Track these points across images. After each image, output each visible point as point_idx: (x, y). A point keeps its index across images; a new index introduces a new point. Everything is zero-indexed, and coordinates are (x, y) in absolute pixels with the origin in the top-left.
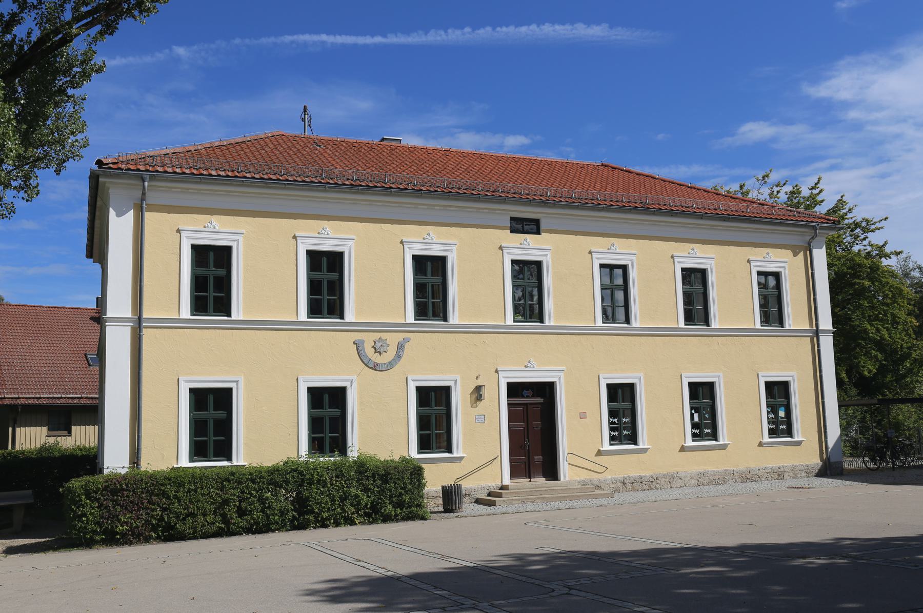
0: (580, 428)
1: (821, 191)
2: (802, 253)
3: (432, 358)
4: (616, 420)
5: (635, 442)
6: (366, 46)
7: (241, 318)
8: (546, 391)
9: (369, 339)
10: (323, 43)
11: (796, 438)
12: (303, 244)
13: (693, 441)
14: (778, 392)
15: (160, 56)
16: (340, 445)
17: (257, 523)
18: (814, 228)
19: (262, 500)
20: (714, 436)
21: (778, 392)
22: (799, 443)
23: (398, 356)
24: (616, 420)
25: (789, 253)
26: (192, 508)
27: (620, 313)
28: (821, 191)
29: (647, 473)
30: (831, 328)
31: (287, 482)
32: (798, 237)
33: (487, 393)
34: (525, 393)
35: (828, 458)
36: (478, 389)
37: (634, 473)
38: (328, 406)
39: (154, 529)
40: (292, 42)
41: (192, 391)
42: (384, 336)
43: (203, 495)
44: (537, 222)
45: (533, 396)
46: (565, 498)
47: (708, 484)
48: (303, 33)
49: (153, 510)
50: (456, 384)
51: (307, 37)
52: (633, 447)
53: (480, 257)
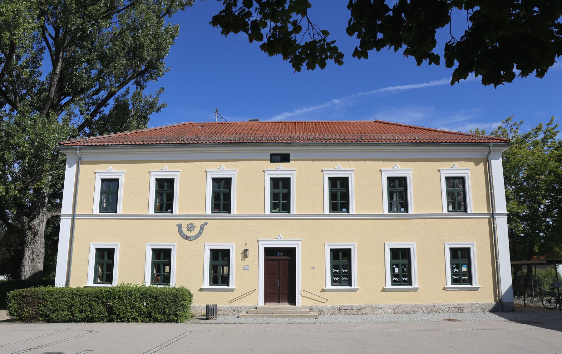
0: (313, 273)
1: (556, 126)
2: (482, 163)
3: (221, 233)
4: (338, 271)
5: (410, 284)
6: (419, 89)
7: (235, 214)
8: (291, 253)
9: (185, 224)
10: (399, 89)
11: (474, 286)
12: (210, 175)
13: (332, 285)
14: (461, 256)
15: (328, 104)
16: (167, 279)
17: (88, 317)
18: (489, 146)
19: (90, 305)
20: (410, 282)
21: (461, 256)
22: (476, 289)
23: (200, 233)
24: (338, 271)
25: (472, 164)
26: (57, 307)
27: (462, 208)
28: (556, 126)
29: (356, 304)
30: (506, 212)
31: (103, 297)
32: (480, 153)
33: (250, 253)
34: (279, 254)
35: (500, 301)
36: (246, 250)
37: (347, 304)
38: (162, 258)
39: (41, 316)
40: (385, 91)
41: (332, 250)
42: (193, 222)
43: (63, 301)
44: (288, 155)
45: (283, 256)
46: (292, 317)
47: (402, 313)
48: (389, 87)
49: (40, 307)
50: (473, 247)
51: (391, 88)
52: (226, 287)
53: (252, 178)
